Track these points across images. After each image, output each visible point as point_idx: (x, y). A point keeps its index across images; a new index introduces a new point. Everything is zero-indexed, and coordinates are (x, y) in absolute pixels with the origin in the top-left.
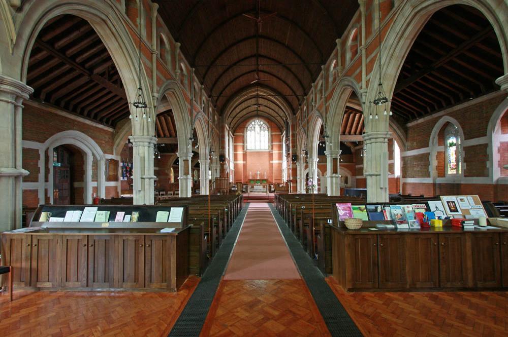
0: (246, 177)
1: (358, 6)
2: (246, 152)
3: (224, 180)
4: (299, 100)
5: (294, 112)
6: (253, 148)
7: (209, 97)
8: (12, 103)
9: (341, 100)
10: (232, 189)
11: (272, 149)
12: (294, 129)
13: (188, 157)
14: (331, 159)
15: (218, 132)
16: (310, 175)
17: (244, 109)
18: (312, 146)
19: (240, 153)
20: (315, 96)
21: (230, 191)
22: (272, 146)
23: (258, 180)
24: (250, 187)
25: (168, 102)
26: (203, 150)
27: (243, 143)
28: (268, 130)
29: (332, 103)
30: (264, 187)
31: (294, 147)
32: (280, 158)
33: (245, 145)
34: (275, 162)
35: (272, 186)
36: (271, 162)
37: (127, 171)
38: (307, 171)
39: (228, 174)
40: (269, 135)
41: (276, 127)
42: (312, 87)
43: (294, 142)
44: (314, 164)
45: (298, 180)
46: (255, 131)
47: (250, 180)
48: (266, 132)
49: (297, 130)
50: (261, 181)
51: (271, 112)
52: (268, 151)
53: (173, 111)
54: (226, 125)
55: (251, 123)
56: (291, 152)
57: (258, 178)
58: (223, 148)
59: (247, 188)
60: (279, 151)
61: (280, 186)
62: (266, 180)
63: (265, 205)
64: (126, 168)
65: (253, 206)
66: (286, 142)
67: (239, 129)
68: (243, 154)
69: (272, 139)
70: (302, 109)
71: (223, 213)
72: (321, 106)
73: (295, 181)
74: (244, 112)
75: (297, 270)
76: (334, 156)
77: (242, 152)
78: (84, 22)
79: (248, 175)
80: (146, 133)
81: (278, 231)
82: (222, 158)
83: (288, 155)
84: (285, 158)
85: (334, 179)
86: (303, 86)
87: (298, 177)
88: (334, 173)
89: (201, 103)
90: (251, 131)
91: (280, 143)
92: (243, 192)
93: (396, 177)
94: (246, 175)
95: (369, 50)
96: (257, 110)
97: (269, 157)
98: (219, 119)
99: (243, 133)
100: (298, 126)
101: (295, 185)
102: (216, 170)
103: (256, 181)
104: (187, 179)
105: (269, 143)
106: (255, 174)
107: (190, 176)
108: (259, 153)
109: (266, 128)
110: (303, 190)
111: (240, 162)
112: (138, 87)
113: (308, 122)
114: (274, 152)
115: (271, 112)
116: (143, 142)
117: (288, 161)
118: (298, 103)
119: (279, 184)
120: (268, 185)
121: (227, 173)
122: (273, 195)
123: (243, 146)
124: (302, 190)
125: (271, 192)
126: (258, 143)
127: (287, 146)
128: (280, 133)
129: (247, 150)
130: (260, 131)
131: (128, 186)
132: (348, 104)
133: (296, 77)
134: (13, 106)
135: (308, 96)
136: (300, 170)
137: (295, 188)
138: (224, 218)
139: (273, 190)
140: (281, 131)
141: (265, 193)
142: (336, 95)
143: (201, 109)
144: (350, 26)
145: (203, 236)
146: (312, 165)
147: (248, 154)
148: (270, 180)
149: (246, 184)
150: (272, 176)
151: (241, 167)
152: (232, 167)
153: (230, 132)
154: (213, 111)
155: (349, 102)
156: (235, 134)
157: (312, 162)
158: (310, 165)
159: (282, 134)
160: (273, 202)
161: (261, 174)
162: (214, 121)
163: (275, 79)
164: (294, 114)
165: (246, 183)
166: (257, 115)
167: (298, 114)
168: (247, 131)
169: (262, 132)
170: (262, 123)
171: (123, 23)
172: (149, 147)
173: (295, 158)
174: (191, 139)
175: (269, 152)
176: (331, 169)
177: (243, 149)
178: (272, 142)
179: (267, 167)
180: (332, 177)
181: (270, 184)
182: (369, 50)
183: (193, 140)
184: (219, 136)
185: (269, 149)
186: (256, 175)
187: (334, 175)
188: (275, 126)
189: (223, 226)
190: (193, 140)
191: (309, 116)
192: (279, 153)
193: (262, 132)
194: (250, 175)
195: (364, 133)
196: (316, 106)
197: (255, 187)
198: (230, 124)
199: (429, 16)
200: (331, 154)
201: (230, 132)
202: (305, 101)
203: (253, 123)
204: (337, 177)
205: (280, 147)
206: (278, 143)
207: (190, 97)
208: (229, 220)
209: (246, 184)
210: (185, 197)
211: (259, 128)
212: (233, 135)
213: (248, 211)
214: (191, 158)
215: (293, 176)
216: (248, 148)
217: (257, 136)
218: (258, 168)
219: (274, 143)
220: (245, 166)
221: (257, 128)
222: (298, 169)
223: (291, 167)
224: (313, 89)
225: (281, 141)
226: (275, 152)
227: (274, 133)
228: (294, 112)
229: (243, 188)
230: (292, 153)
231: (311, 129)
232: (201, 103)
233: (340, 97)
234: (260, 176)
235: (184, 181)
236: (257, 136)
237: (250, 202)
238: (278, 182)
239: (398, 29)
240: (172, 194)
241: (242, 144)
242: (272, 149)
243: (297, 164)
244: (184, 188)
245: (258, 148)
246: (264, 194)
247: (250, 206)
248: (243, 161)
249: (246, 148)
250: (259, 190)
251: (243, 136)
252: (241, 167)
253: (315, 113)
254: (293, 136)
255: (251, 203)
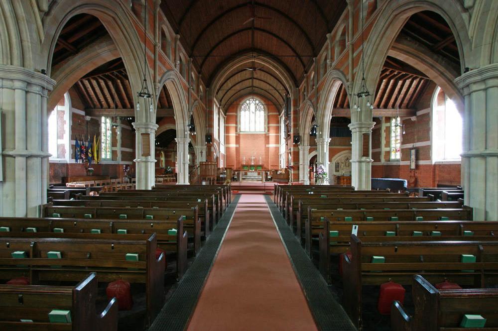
0: (238, 162)
1: (346, 4)
2: (239, 134)
3: (211, 164)
4: (304, 66)
5: (297, 84)
6: (247, 130)
7: (190, 57)
8: (40, 94)
9: (384, 39)
10: (221, 176)
11: (269, 131)
12: (296, 104)
13: (149, 130)
14: (360, 135)
15: (204, 106)
16: (320, 160)
17: (237, 84)
18: (323, 122)
19: (232, 135)
20: (331, 53)
21: (218, 177)
22: (268, 127)
23: (253, 166)
24: (241, 173)
25: (113, 43)
26: (181, 125)
27: (236, 124)
28: (265, 111)
29: (368, 47)
30: (259, 174)
31: (296, 126)
32: (278, 141)
33: (239, 126)
34: (272, 145)
35: (269, 173)
36: (267, 146)
37: (82, 152)
38: (313, 154)
39: (217, 158)
40: (265, 116)
41: (273, 106)
42: (327, 39)
43: (296, 120)
44: (325, 145)
45: (301, 167)
46: (249, 111)
47: (244, 166)
48: (262, 113)
49: (301, 106)
50: (256, 167)
51: (268, 87)
52: (264, 133)
53: (127, 66)
54: (215, 100)
55: (245, 102)
56: (292, 133)
57: (253, 164)
58: (211, 126)
59: (238, 174)
60: (276, 133)
61: (279, 173)
62: (262, 166)
63: (260, 199)
64: (81, 147)
65: (246, 199)
66: (285, 121)
67: (231, 109)
68: (236, 137)
69: (269, 120)
70: (308, 77)
71: (202, 209)
72: (341, 63)
73: (296, 168)
74: (238, 87)
75: (302, 290)
76: (364, 131)
77: (235, 135)
78: (94, 19)
79: (241, 160)
80: (17, 61)
81: (287, 280)
82: (209, 138)
83: (288, 136)
84: (283, 141)
85: (364, 165)
86: (310, 43)
87: (301, 162)
88: (364, 156)
89: (175, 59)
90: (245, 111)
91: (277, 125)
92: (233, 179)
93: (433, 163)
94: (239, 160)
95: (354, 47)
96: (252, 86)
97: (266, 140)
98: (205, 91)
99: (236, 113)
100: (301, 101)
101: (296, 172)
102: (202, 152)
103: (250, 166)
104: (146, 162)
105: (265, 124)
106: (249, 159)
107: (152, 158)
108: (253, 136)
109: (262, 107)
110: (306, 178)
111: (233, 145)
112: (143, 79)
113: (318, 90)
114: (270, 135)
115: (268, 87)
116: (12, 80)
117: (287, 145)
118: (303, 70)
119: (277, 171)
120: (264, 172)
121: (217, 157)
122: (271, 184)
123: (236, 128)
124: (305, 179)
125: (267, 180)
126: (252, 124)
127: (287, 126)
128: (278, 114)
129: (240, 132)
130: (256, 111)
131: (85, 170)
132: (393, 54)
133: (303, 32)
134: (24, 92)
135: (308, 74)
136: (304, 154)
137: (297, 177)
138: (212, 207)
139: (269, 177)
140: (279, 112)
141: (261, 182)
142: (373, 36)
143: (176, 67)
144: (339, 22)
145: (197, 218)
146: (323, 147)
147: (241, 136)
148: (265, 166)
149: (238, 170)
150: (268, 162)
151: (233, 151)
152: (222, 150)
153: (221, 110)
154: (197, 78)
155: (394, 48)
156: (227, 114)
157: (323, 142)
158: (319, 147)
159: (280, 115)
160: (271, 194)
161: (256, 159)
162: (198, 91)
163: (275, 41)
164: (297, 86)
165: (237, 169)
166: (253, 92)
167: (303, 85)
168: (240, 110)
169: (258, 112)
170: (257, 102)
171: (129, 17)
172: (27, 92)
173: (297, 140)
174: (189, 126)
175: (265, 134)
176: (359, 150)
177: (236, 131)
178: (269, 123)
179: (262, 150)
180: (360, 162)
181: (266, 170)
182: (354, 47)
183: (190, 127)
184: (205, 111)
185: (265, 131)
186: (251, 160)
187: (364, 159)
188: (272, 104)
189: (211, 215)
190: (190, 127)
191: (320, 82)
192: (276, 136)
193: (258, 112)
194: (244, 160)
195: (467, 70)
196: (333, 64)
197: (249, 174)
198: (221, 101)
199: (407, 18)
200: (360, 128)
201: (221, 110)
202: (305, 80)
203: (248, 102)
204: (369, 162)
205: (278, 129)
206: (275, 125)
207: (153, 42)
208: (215, 218)
209: (238, 170)
210: (143, 188)
211: (254, 109)
212: (225, 115)
213: (236, 210)
214: (154, 131)
215: (294, 161)
216: (242, 130)
217: (253, 117)
218: (252, 152)
219: (270, 125)
220: (237, 150)
221: (252, 106)
222: (301, 153)
223: (292, 150)
224: (328, 41)
225: (278, 122)
226: (272, 135)
227: (270, 114)
228: (297, 84)
229: (234, 174)
230: (294, 134)
231: (323, 98)
232: (175, 59)
233: (384, 33)
234: (254, 161)
235: (143, 165)
236: (253, 117)
237: (242, 194)
238: (275, 168)
239: (379, 29)
240: (127, 182)
241: (234, 125)
242: (269, 131)
243: (300, 147)
244: (143, 176)
245: (252, 130)
246: (259, 183)
247: (240, 201)
248: (236, 144)
249: (240, 129)
250: (253, 179)
251: (236, 117)
252: (233, 151)
253: (332, 73)
254: (296, 112)
255: (242, 195)
